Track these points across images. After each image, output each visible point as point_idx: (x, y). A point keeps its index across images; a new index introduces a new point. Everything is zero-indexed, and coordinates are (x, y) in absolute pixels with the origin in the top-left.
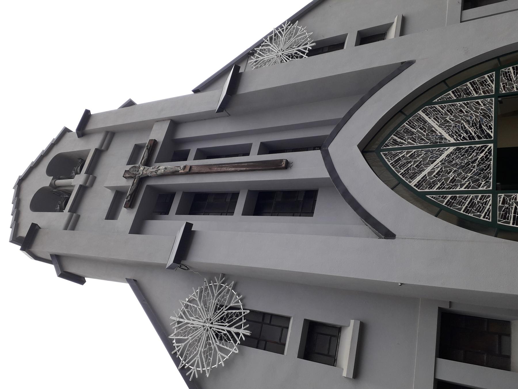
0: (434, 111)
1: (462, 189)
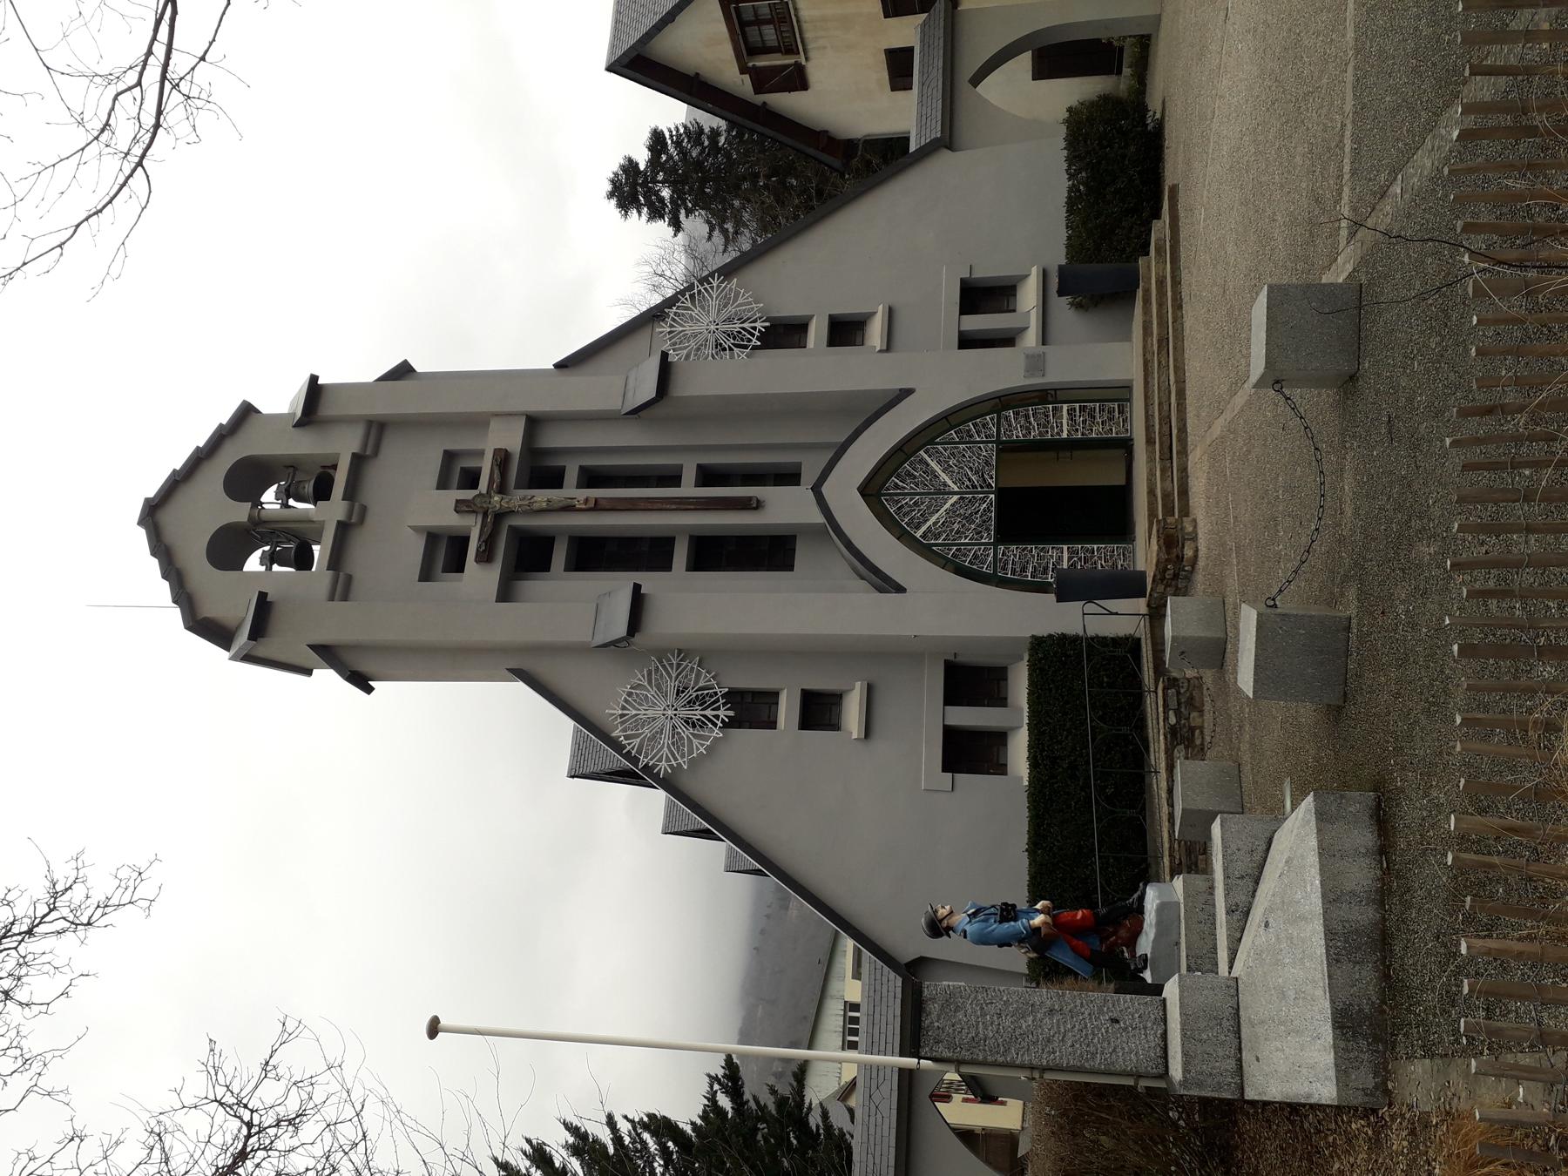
1: (967, 541)
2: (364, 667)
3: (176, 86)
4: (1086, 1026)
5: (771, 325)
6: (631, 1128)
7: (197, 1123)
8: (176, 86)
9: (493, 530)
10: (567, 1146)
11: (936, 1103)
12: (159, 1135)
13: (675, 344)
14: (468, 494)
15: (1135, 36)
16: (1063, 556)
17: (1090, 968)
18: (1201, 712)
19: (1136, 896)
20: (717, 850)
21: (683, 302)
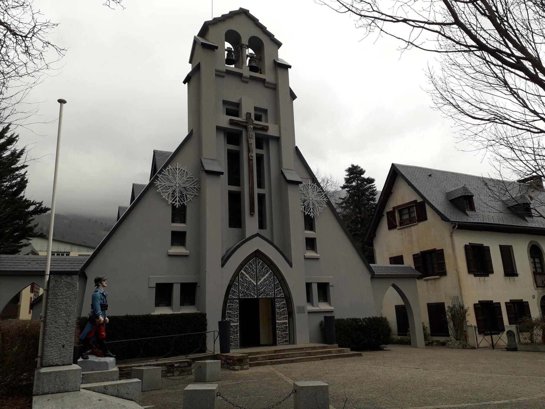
0: (271, 276)
1: (240, 288)
2: (193, 81)
3: (373, 22)
4: (61, 336)
5: (312, 218)
6: (22, 174)
7: (27, 18)
8: (373, 22)
9: (241, 125)
10: (15, 150)
11: (30, 285)
12: (23, 5)
13: (305, 186)
14: (253, 117)
15: (410, 339)
16: (235, 323)
17: (83, 338)
18: (179, 375)
19: (111, 354)
20: (127, 204)
21: (318, 189)
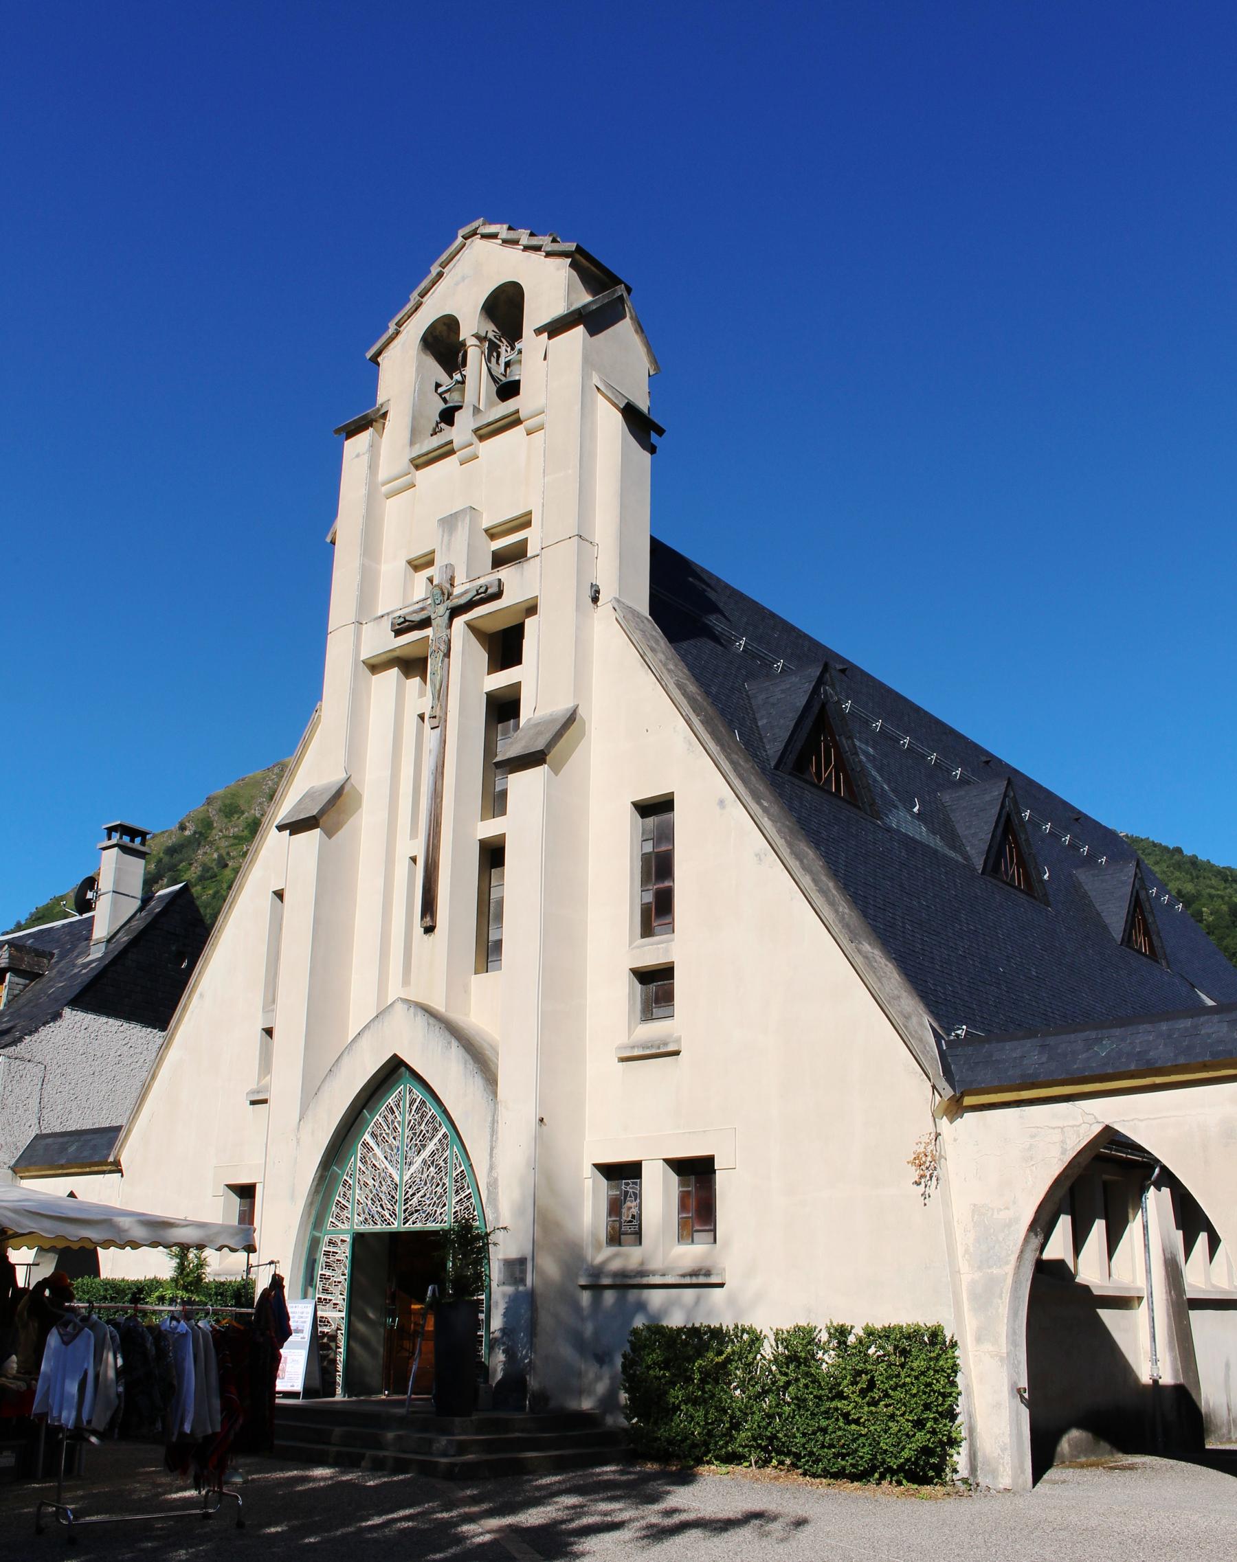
1: (357, 1197)
